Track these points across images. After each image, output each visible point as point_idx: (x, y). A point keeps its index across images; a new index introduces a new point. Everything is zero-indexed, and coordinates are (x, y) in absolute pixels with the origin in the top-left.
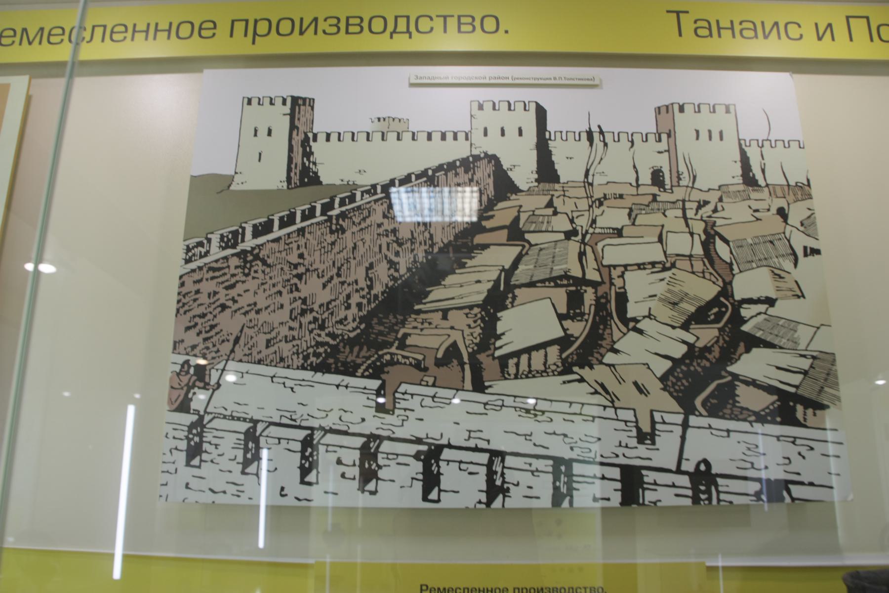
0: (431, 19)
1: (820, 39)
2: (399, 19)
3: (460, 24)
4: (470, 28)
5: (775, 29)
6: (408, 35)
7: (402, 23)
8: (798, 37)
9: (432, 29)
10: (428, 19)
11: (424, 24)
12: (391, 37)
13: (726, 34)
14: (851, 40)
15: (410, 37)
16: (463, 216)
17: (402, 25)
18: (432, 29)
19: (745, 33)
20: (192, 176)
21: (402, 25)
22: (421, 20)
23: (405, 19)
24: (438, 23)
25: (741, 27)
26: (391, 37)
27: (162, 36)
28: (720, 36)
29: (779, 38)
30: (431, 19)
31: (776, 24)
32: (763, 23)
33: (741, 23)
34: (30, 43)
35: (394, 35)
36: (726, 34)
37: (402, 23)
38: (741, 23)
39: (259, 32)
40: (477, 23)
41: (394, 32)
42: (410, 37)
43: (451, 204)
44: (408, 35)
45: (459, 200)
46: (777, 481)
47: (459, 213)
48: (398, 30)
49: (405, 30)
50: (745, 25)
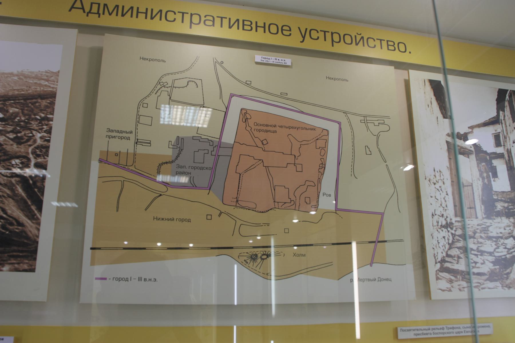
0: (175, 13)
1: (230, 27)
2: (93, 5)
3: (388, 45)
4: (249, 28)
5: (362, 40)
6: (97, 15)
7: (95, 7)
8: (373, 46)
9: (175, 19)
10: (173, 13)
11: (171, 16)
12: (87, 16)
13: (142, 16)
14: (222, 26)
15: (99, 17)
16: (187, 123)
17: (95, 9)
18: (175, 19)
19: (207, 22)
20: (500, 90)
21: (95, 9)
22: (168, 13)
23: (97, 5)
24: (179, 16)
25: (205, 19)
26: (87, 16)
27: (261, 30)
28: (137, 17)
29: (364, 45)
30: (175, 13)
31: (238, 20)
32: (152, 10)
33: (205, 17)
34: (110, 14)
35: (89, 14)
36: (142, 16)
37: (95, 7)
38: (205, 17)
39: (193, 21)
40: (396, 46)
41: (90, 12)
42: (99, 17)
43: (194, 116)
44: (97, 15)
45: (199, 115)
46: (477, 160)
47: (198, 122)
48: (92, 12)
49: (96, 12)
50: (208, 18)
